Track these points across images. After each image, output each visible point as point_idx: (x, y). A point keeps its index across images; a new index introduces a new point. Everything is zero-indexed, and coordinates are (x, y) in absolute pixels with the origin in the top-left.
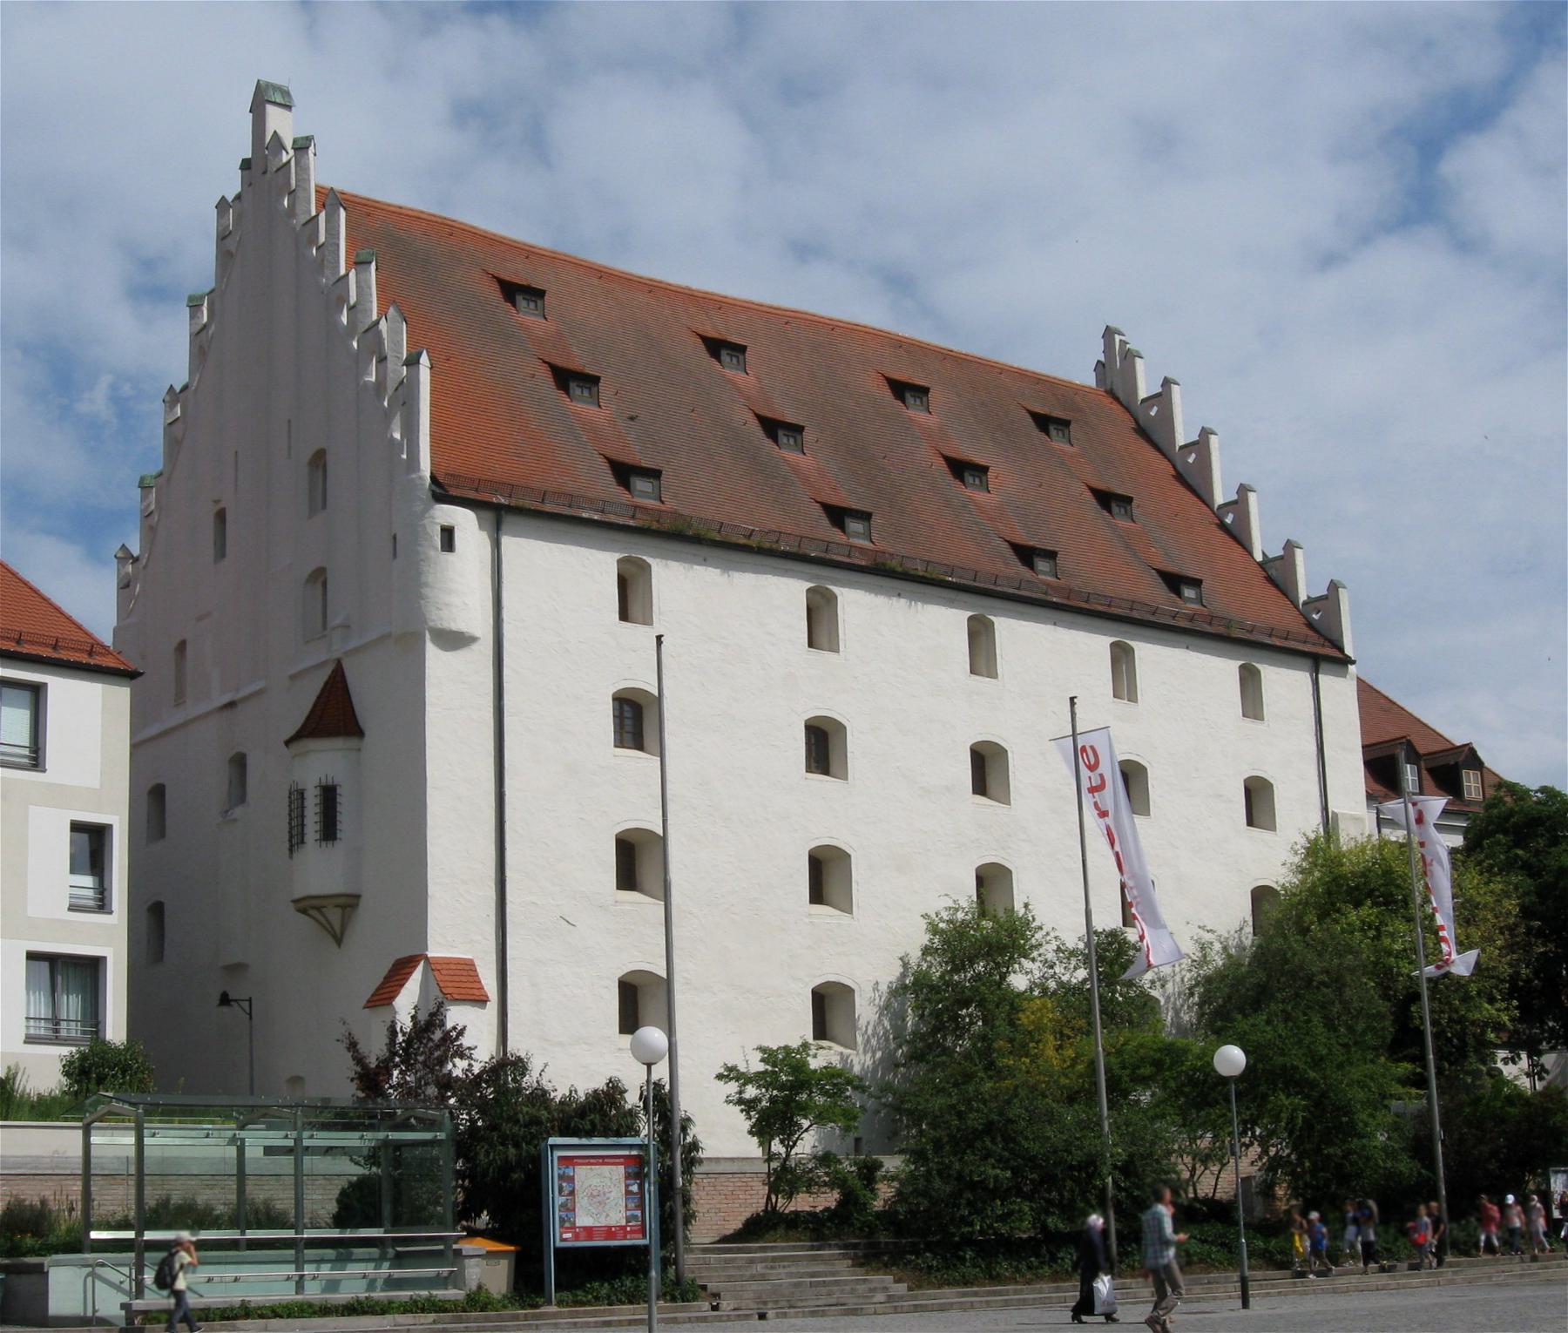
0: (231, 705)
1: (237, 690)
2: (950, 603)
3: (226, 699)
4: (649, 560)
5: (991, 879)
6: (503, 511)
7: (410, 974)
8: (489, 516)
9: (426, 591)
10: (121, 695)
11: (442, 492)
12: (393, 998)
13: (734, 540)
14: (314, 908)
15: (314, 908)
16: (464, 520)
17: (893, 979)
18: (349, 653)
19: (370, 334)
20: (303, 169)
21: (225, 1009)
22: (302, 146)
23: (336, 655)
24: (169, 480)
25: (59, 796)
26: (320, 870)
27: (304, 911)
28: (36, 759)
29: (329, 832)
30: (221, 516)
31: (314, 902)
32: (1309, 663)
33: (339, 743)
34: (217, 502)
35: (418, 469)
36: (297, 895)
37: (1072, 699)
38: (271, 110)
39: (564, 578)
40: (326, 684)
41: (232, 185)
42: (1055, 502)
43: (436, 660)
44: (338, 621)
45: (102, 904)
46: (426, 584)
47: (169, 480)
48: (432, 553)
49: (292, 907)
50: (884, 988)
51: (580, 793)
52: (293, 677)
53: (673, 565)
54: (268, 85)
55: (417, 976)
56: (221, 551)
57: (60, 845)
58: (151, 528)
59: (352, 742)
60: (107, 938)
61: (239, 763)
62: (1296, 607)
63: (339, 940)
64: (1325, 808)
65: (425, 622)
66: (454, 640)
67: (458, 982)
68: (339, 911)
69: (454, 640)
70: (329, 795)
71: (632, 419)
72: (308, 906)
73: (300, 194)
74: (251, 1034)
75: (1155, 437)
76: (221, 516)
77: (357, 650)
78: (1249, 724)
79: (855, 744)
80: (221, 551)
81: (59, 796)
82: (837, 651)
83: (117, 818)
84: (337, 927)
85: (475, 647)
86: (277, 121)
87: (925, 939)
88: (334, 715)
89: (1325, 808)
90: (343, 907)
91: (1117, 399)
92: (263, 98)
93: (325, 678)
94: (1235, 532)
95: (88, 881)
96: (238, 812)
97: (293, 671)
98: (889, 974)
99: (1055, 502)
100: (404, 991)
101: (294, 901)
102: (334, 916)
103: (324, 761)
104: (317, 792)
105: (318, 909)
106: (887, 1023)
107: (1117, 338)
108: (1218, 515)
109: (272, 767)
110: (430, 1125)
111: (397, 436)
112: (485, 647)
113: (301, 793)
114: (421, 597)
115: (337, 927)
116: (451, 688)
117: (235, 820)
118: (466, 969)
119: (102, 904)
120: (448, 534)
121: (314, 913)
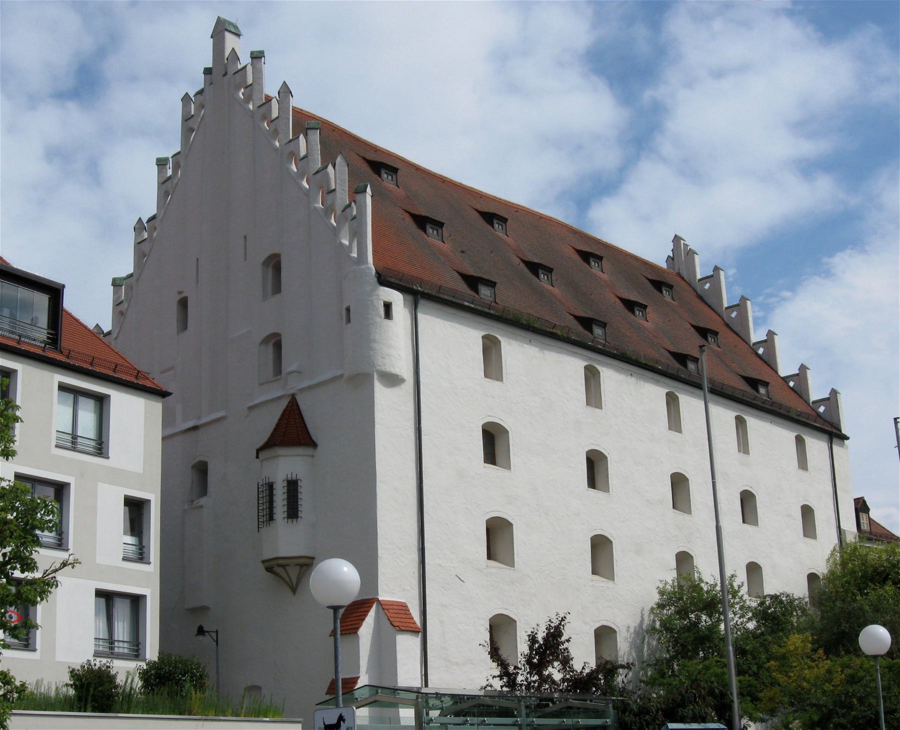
0: (195, 428)
1: (199, 418)
2: (657, 383)
3: (190, 424)
4: (500, 338)
5: (684, 559)
6: (417, 295)
7: (368, 611)
8: (410, 298)
9: (374, 345)
10: (156, 407)
11: (383, 280)
12: (358, 628)
13: (544, 328)
14: (279, 566)
15: (279, 566)
16: (396, 298)
17: (637, 625)
18: (302, 390)
19: (319, 175)
20: (258, 74)
21: (201, 638)
22: (257, 56)
23: (292, 392)
24: (138, 280)
25: (116, 477)
26: (286, 539)
27: (269, 569)
28: (101, 448)
29: (293, 512)
30: (183, 303)
31: (281, 562)
32: (826, 437)
33: (300, 450)
34: (180, 293)
35: (367, 262)
36: (265, 558)
37: (895, 419)
38: (228, 37)
39: (451, 342)
40: (285, 411)
41: (198, 82)
42: (678, 331)
43: (382, 395)
44: (294, 367)
45: (141, 556)
46: (374, 341)
47: (138, 280)
48: (378, 320)
49: (261, 566)
50: (632, 630)
51: (465, 492)
52: (251, 408)
53: (514, 342)
54: (225, 21)
55: (372, 613)
56: (183, 324)
57: (118, 515)
58: (122, 313)
59: (309, 451)
60: (145, 581)
61: (202, 469)
62: (809, 404)
63: (294, 590)
64: (839, 527)
65: (374, 366)
66: (392, 380)
67: (398, 619)
68: (298, 567)
69: (392, 380)
70: (293, 486)
71: (463, 252)
72: (274, 566)
73: (256, 87)
74: (217, 659)
75: (706, 300)
76: (183, 303)
77: (310, 388)
78: (801, 472)
79: (615, 469)
80: (183, 324)
81: (116, 477)
82: (601, 408)
83: (153, 495)
84: (294, 583)
85: (403, 386)
86: (231, 42)
87: (656, 598)
88: (292, 431)
89: (839, 527)
90: (301, 566)
91: (683, 278)
92: (221, 29)
93: (284, 407)
94: (765, 358)
95: (130, 539)
96: (203, 501)
97: (252, 404)
98: (634, 623)
99: (678, 331)
100: (364, 624)
101: (263, 562)
102: (293, 572)
103: (287, 464)
104: (285, 484)
105: (283, 566)
106: (634, 654)
107: (682, 242)
108: (753, 348)
109: (271, 460)
110: (598, 714)
111: (346, 243)
112: (409, 385)
113: (271, 487)
114: (371, 349)
115: (294, 583)
116: (390, 408)
117: (201, 507)
118: (403, 608)
119: (141, 556)
120: (388, 307)
121: (280, 570)
